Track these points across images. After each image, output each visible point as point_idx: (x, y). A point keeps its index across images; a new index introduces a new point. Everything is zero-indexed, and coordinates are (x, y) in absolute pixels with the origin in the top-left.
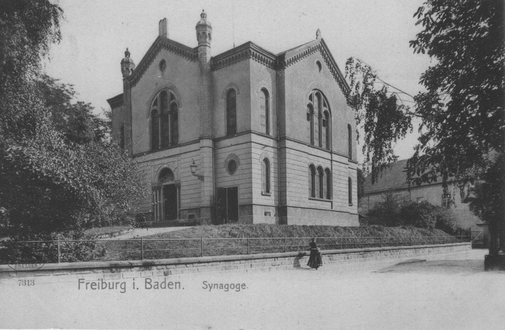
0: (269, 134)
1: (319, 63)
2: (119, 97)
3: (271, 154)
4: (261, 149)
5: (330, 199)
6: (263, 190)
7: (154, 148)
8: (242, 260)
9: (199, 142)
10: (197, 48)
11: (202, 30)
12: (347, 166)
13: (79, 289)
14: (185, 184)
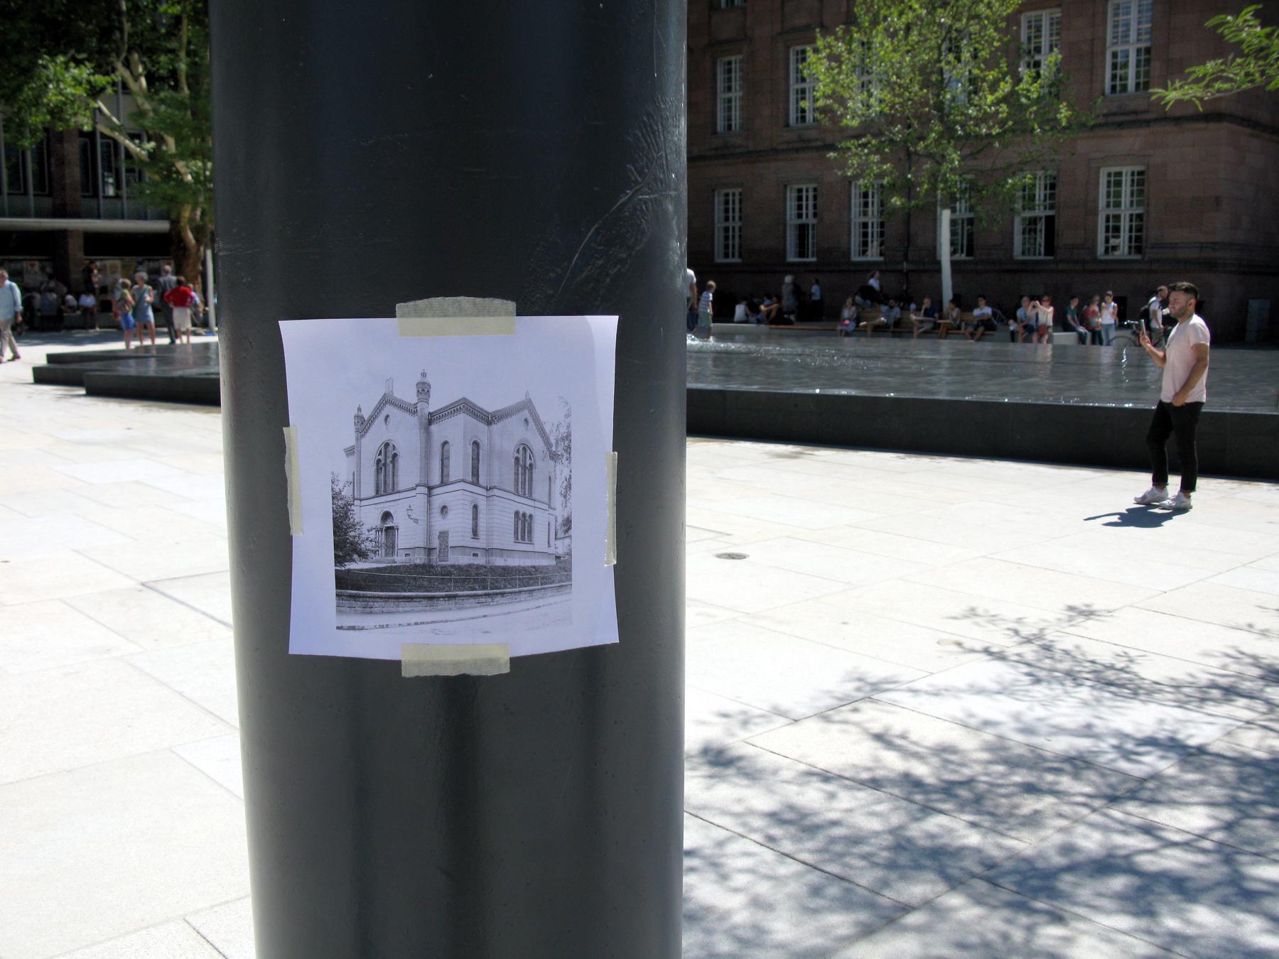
1: (526, 420)
2: (353, 448)
11: (424, 390)
13: (720, 556)
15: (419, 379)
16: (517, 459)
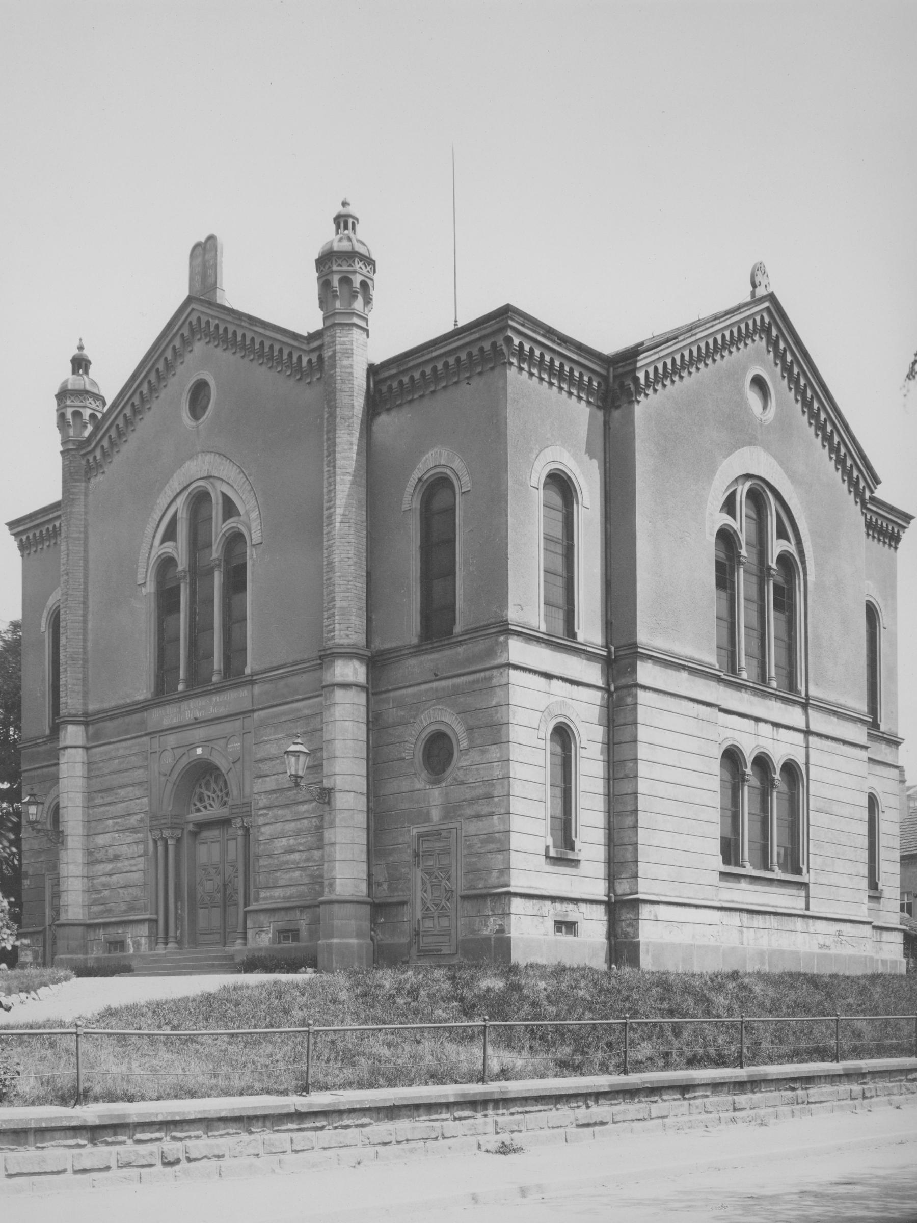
3: (585, 712)
4: (543, 692)
5: (799, 872)
6: (550, 842)
10: (318, 335)
11: (342, 274)
12: (864, 755)
14: (264, 801)
15: (325, 236)
16: (726, 537)
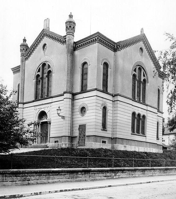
0: (107, 91)
1: (141, 49)
2: (19, 67)
7: (36, 99)
8: (152, 169)
9: (63, 95)
10: (66, 36)
11: (71, 26)
